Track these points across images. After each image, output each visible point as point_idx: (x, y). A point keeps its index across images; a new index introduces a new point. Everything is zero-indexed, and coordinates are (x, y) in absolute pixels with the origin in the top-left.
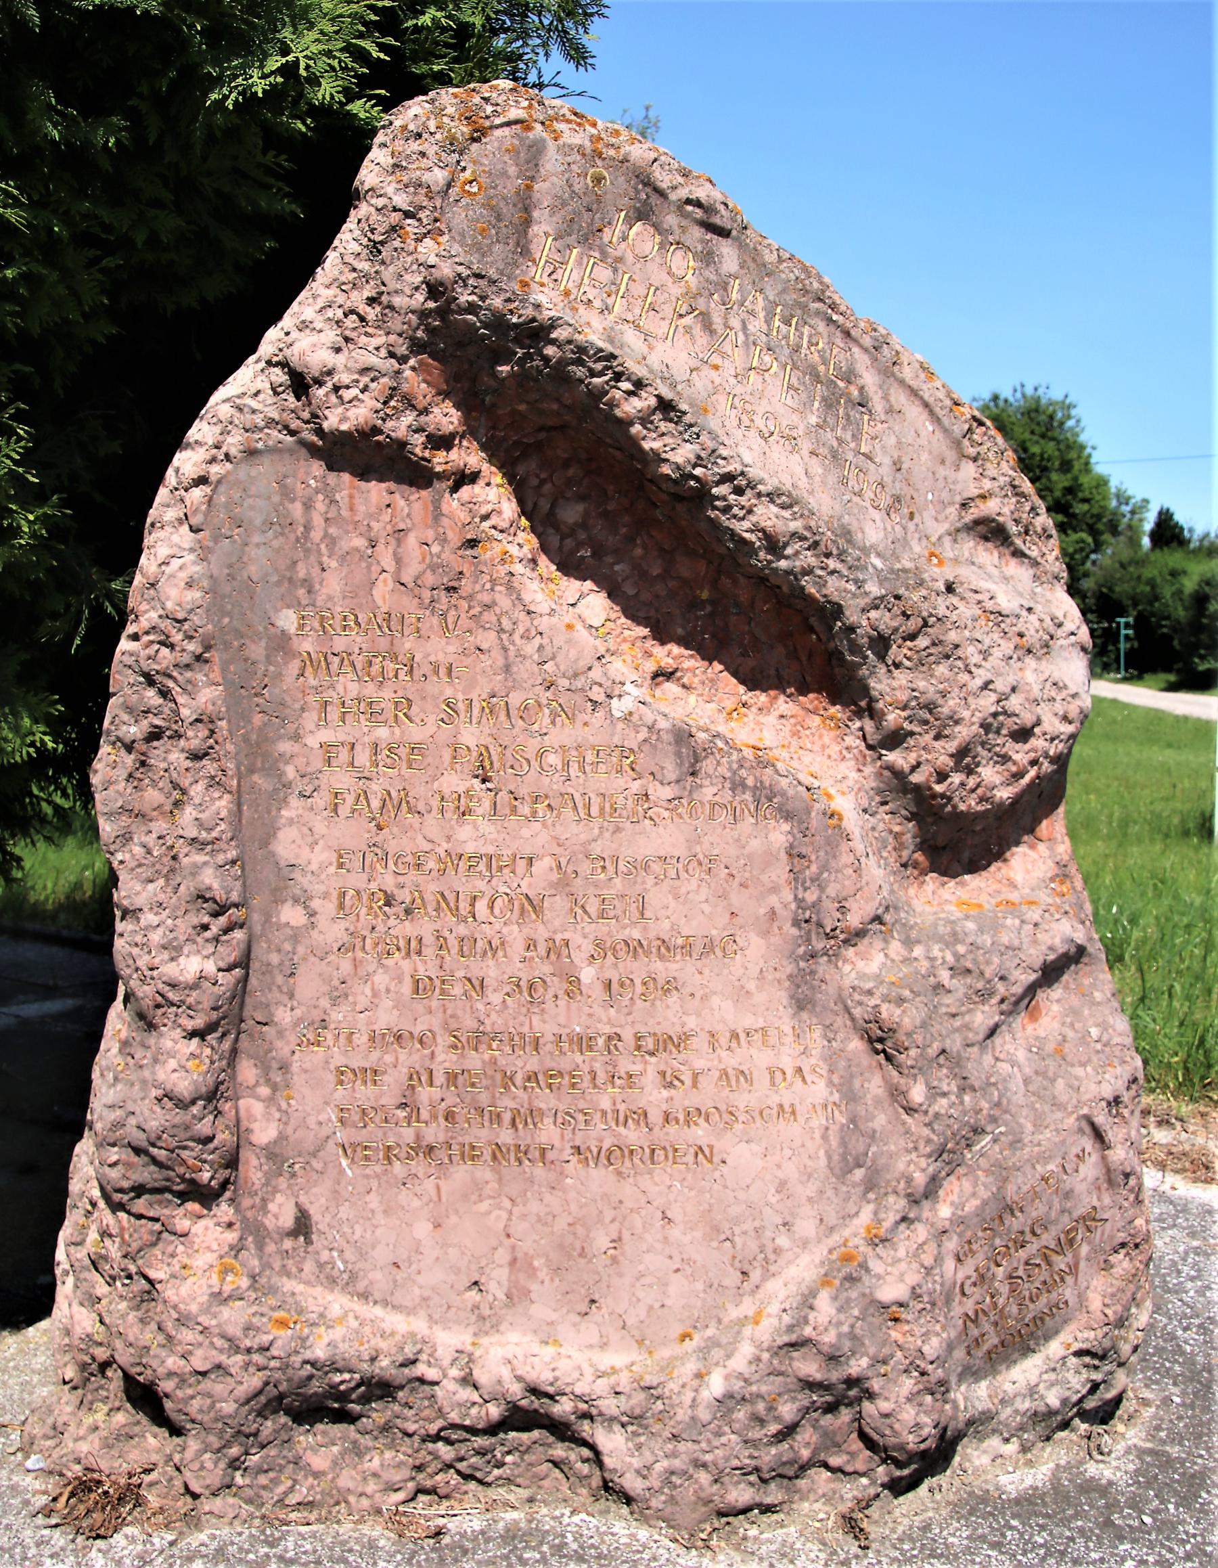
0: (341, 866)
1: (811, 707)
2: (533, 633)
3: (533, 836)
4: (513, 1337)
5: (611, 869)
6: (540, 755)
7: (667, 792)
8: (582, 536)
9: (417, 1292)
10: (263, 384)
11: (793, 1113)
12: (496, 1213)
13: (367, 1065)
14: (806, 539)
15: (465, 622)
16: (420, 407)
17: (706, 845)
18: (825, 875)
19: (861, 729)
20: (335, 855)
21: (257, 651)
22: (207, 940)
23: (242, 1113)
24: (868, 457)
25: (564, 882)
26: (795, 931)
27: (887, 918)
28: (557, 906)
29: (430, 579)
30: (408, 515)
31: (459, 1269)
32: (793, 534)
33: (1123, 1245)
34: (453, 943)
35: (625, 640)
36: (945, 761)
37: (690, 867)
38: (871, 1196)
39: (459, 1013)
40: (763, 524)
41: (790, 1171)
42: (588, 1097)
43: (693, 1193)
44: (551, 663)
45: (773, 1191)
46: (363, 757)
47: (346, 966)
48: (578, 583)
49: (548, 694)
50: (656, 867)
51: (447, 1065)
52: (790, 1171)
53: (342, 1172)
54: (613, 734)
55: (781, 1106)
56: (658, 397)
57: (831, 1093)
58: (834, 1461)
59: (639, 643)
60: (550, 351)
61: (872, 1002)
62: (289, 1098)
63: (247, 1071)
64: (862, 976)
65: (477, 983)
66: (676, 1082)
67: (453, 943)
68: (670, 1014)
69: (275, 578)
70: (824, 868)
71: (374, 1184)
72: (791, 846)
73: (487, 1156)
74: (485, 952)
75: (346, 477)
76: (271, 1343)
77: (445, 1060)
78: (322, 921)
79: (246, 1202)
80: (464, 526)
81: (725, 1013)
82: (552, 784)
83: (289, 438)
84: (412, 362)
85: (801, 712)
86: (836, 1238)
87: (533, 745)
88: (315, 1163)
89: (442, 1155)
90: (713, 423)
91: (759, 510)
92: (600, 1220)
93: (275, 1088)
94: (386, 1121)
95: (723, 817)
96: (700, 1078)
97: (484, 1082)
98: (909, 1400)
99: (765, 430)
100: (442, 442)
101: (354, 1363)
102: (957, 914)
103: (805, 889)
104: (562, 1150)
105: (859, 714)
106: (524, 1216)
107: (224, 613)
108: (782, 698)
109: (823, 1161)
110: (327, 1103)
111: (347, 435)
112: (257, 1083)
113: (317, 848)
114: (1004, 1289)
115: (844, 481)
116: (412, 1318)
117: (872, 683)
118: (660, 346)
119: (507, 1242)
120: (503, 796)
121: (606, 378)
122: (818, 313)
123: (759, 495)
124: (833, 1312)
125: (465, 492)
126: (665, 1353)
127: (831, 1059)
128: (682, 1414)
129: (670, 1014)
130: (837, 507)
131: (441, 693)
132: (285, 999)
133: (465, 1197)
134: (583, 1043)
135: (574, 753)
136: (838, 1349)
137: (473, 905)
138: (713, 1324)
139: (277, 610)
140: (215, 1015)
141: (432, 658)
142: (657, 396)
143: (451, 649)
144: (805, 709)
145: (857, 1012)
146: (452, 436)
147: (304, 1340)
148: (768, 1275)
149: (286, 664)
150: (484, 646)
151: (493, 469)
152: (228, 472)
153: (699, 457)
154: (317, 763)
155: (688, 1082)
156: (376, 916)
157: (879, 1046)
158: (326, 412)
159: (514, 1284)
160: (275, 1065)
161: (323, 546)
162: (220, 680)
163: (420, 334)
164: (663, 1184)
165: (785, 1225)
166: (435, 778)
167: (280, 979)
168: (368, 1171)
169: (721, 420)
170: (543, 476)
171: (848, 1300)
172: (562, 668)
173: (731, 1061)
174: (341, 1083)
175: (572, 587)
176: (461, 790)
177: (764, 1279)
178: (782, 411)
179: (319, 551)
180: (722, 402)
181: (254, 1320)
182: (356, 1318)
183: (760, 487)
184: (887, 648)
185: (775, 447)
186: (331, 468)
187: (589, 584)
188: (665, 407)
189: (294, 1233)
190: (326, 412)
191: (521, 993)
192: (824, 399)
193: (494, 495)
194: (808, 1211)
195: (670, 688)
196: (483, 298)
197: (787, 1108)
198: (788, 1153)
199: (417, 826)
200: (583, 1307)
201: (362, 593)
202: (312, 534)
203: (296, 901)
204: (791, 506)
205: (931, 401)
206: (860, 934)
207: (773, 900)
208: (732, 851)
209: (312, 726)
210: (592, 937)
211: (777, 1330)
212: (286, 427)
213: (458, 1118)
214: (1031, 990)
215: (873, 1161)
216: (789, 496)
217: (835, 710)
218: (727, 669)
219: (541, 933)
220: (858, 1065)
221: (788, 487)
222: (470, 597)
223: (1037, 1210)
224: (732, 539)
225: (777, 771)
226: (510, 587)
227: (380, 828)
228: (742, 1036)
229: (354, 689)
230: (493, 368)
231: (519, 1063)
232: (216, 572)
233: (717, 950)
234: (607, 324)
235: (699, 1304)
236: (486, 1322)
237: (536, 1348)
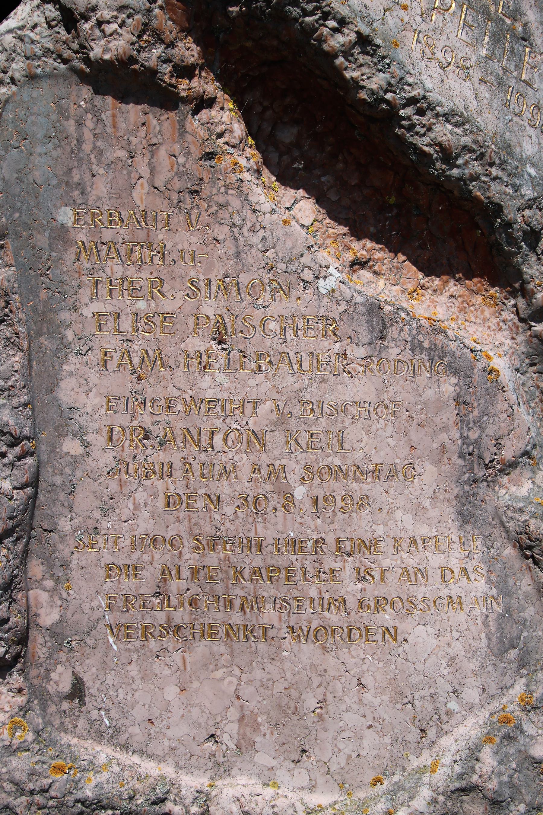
0: (110, 408)
1: (475, 289)
2: (258, 227)
3: (258, 385)
4: (242, 780)
5: (317, 410)
6: (263, 322)
7: (361, 352)
8: (296, 153)
9: (167, 743)
10: (38, 18)
11: (460, 603)
12: (229, 679)
13: (130, 563)
14: (474, 151)
15: (204, 218)
16: (167, 41)
17: (391, 393)
18: (485, 418)
19: (515, 306)
20: (105, 400)
21: (42, 240)
22: (5, 465)
23: (32, 601)
24: (528, 83)
25: (281, 420)
26: (460, 462)
27: (535, 453)
28: (276, 438)
29: (177, 184)
30: (160, 132)
31: (200, 724)
34: (196, 467)
35: (329, 236)
37: (379, 410)
38: (524, 672)
39: (201, 522)
40: (440, 139)
41: (458, 648)
42: (300, 588)
43: (381, 665)
44: (272, 251)
45: (445, 665)
46: (126, 325)
47: (114, 486)
48: (293, 191)
49: (269, 275)
50: (353, 410)
51: (191, 562)
52: (458, 648)
53: (109, 647)
54: (319, 307)
55: (450, 597)
56: (358, 33)
57: (490, 589)
59: (340, 239)
61: (523, 518)
62: (69, 589)
63: (36, 568)
64: (514, 498)
65: (214, 498)
66: (368, 577)
67: (196, 467)
68: (363, 524)
69: (55, 182)
70: (484, 412)
71: (135, 656)
72: (458, 395)
73: (222, 634)
74: (221, 475)
75: (109, 99)
76: (50, 786)
77: (190, 558)
78: (95, 451)
79: (33, 672)
80: (204, 141)
81: (406, 523)
82: (272, 345)
83: (62, 66)
85: (467, 293)
87: (259, 314)
88: (88, 640)
89: (187, 633)
90: (402, 56)
91: (437, 128)
92: (309, 684)
93: (57, 581)
94: (144, 607)
95: (405, 371)
96: (386, 573)
97: (220, 576)
99: (443, 60)
100: (185, 71)
101: (116, 801)
103: (469, 429)
104: (279, 629)
105: (513, 294)
106: (250, 682)
107: (16, 210)
108: (452, 282)
109: (484, 642)
110: (98, 593)
111: (109, 63)
112: (44, 578)
113: (91, 395)
115: (506, 104)
116: (162, 765)
117: (525, 268)
119: (237, 703)
120: (235, 354)
121: (316, 17)
123: (437, 115)
124: (495, 763)
125: (204, 114)
126: (362, 795)
127: (490, 562)
129: (363, 524)
130: (500, 125)
131: (187, 274)
132: (66, 511)
134: (297, 545)
135: (289, 321)
136: (500, 795)
137: (211, 438)
138: (398, 771)
139: (57, 208)
140: (10, 523)
141: (180, 247)
142: (357, 32)
143: (194, 240)
144: (469, 290)
145: (511, 525)
146: (193, 67)
147: (77, 782)
148: (442, 733)
149: (65, 250)
150: (220, 238)
151: (226, 96)
152: (14, 94)
153: (389, 84)
154: (91, 328)
155: (377, 577)
156: (137, 447)
157: (529, 553)
158: (92, 44)
159: (243, 736)
160: (58, 563)
161: (92, 156)
162: (12, 262)
164: (358, 657)
165: (454, 692)
166: (182, 341)
167: (62, 497)
168: (129, 646)
170: (266, 104)
171: (507, 755)
172: (280, 255)
173: (411, 561)
174: (109, 576)
175: (288, 195)
176: (202, 349)
177: (438, 737)
178: (458, 45)
179: (89, 161)
180: (410, 37)
181: (37, 767)
182: (118, 764)
183: (438, 109)
184: (538, 240)
185: (451, 75)
186: (97, 92)
187: (301, 192)
188: (364, 41)
189: (70, 697)
190: (92, 44)
191: (248, 506)
192: (493, 35)
193: (226, 117)
194: (471, 681)
195: (365, 274)
197: (455, 599)
198: (456, 634)
199: (168, 377)
200: (296, 756)
201: (124, 195)
202: (84, 146)
204: (463, 124)
206: (513, 465)
207: (444, 437)
208: (412, 398)
209: (85, 300)
210: (303, 463)
211: (450, 778)
212: (60, 56)
213: (200, 604)
215: (525, 644)
216: (462, 116)
217: (494, 291)
218: (409, 259)
219: (264, 460)
220: (511, 567)
221: (461, 108)
222: (209, 199)
224: (415, 153)
225: (447, 337)
226: (239, 191)
227: (140, 379)
228: (420, 542)
229: (118, 271)
230: (225, 9)
231: (247, 561)
232: (7, 176)
233: (400, 475)
235: (387, 755)
236: (221, 768)
237: (259, 789)
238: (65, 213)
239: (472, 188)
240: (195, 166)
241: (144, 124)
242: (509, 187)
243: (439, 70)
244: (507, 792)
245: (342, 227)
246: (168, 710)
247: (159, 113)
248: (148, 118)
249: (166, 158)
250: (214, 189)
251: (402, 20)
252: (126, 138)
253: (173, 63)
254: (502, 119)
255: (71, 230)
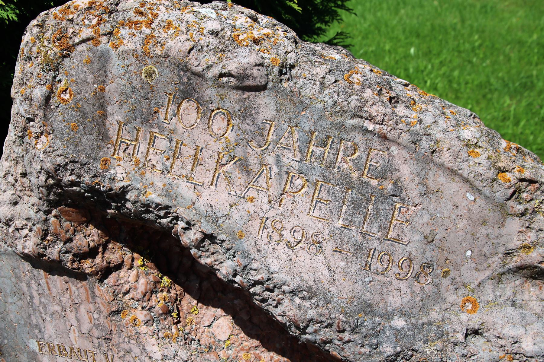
30: (78, 295)
32: (310, 320)
35: (242, 349)
48: (214, 309)
69: (23, 322)
84: (54, 212)
90: (247, 244)
118: (206, 192)
121: (169, 219)
122: (354, 128)
123: (284, 293)
139: (28, 339)
161: (41, 308)
163: (51, 197)
169: (255, 240)
179: (40, 310)
183: (285, 288)
196: (79, 177)
201: (64, 336)
205: (471, 177)
221: (311, 282)
222: (118, 345)
234: (167, 181)
238: (33, 343)
239: (328, 348)
240: (105, 321)
241: (67, 289)
242: (366, 346)
243: (287, 249)
245: (255, 340)
247: (76, 282)
248: (69, 285)
249: (86, 314)
250: (120, 339)
251: (248, 212)
252: (58, 298)
253: (72, 254)
254: (360, 282)
255: (39, 354)
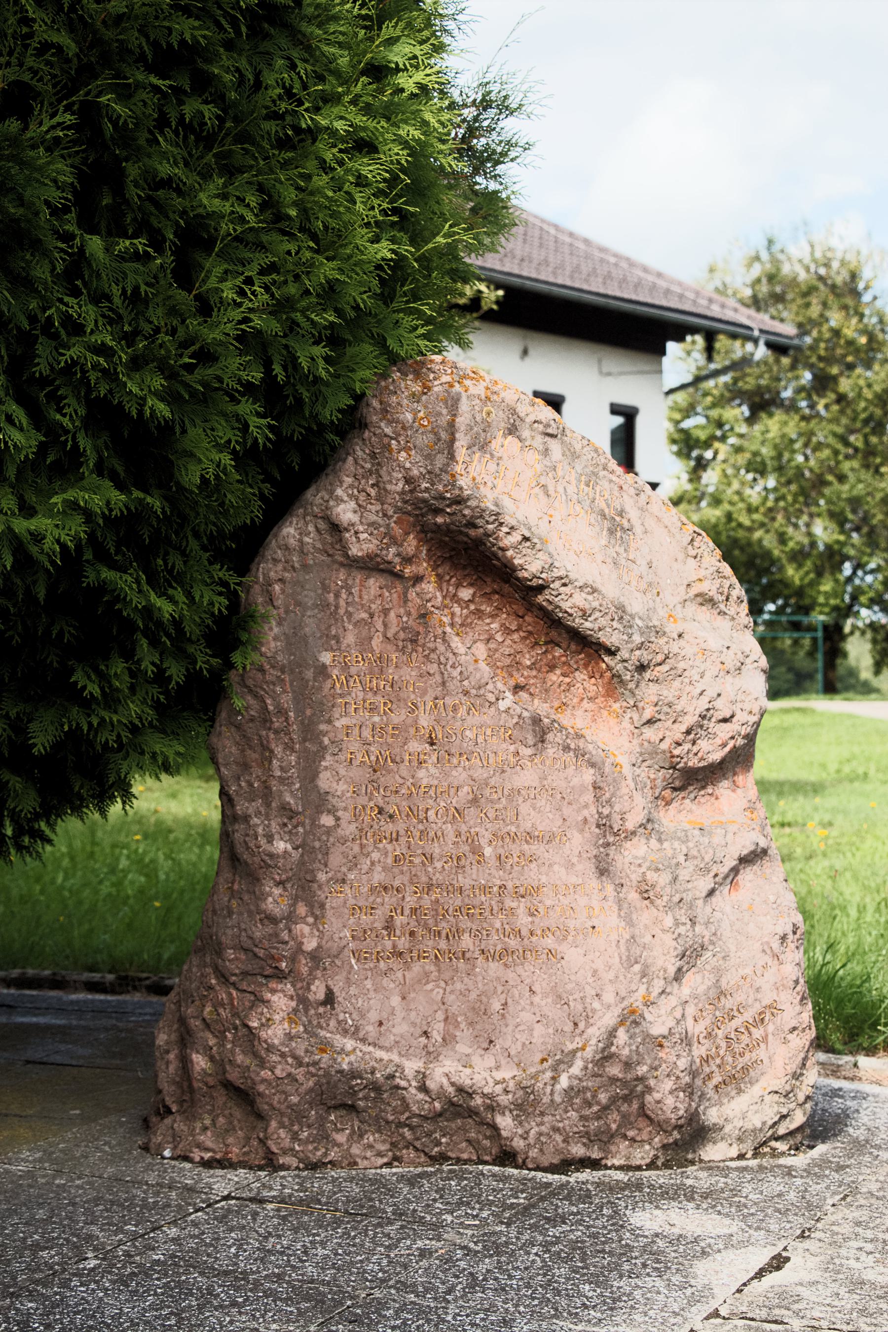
4: (447, 1063)
15: (421, 659)
21: (309, 674)
29: (402, 635)
33: (795, 1029)
36: (679, 737)
46: (367, 733)
47: (356, 849)
53: (352, 967)
58: (631, 1134)
60: (467, 512)
77: (410, 901)
78: (343, 823)
86: (626, 1003)
92: (495, 992)
93: (316, 918)
98: (670, 1093)
100: (408, 560)
102: (688, 827)
106: (452, 992)
109: (617, 960)
114: (723, 1045)
115: (620, 578)
128: (546, 1100)
133: (419, 981)
134: (485, 889)
148: (588, 1025)
167: (320, 856)
169: (555, 545)
177: (586, 1027)
195: (523, 695)
200: (486, 1045)
203: (329, 812)
206: (634, 833)
207: (586, 813)
208: (563, 784)
214: (735, 871)
222: (424, 645)
223: (740, 997)
226: (444, 640)
227: (375, 771)
244: (635, 1058)
246: (393, 1014)
